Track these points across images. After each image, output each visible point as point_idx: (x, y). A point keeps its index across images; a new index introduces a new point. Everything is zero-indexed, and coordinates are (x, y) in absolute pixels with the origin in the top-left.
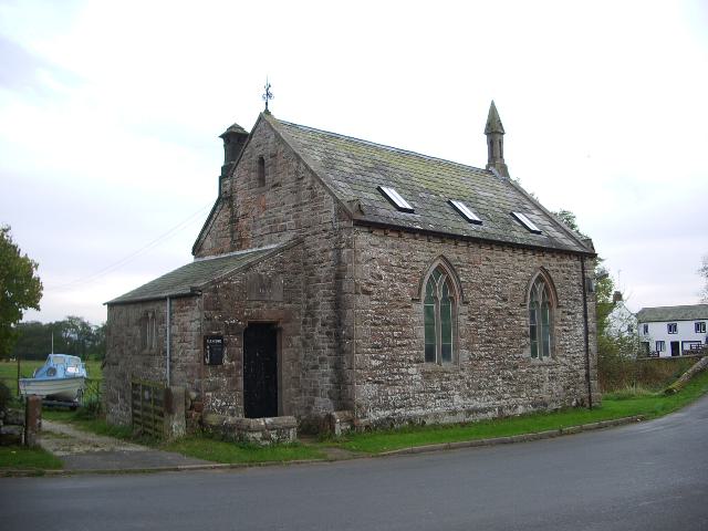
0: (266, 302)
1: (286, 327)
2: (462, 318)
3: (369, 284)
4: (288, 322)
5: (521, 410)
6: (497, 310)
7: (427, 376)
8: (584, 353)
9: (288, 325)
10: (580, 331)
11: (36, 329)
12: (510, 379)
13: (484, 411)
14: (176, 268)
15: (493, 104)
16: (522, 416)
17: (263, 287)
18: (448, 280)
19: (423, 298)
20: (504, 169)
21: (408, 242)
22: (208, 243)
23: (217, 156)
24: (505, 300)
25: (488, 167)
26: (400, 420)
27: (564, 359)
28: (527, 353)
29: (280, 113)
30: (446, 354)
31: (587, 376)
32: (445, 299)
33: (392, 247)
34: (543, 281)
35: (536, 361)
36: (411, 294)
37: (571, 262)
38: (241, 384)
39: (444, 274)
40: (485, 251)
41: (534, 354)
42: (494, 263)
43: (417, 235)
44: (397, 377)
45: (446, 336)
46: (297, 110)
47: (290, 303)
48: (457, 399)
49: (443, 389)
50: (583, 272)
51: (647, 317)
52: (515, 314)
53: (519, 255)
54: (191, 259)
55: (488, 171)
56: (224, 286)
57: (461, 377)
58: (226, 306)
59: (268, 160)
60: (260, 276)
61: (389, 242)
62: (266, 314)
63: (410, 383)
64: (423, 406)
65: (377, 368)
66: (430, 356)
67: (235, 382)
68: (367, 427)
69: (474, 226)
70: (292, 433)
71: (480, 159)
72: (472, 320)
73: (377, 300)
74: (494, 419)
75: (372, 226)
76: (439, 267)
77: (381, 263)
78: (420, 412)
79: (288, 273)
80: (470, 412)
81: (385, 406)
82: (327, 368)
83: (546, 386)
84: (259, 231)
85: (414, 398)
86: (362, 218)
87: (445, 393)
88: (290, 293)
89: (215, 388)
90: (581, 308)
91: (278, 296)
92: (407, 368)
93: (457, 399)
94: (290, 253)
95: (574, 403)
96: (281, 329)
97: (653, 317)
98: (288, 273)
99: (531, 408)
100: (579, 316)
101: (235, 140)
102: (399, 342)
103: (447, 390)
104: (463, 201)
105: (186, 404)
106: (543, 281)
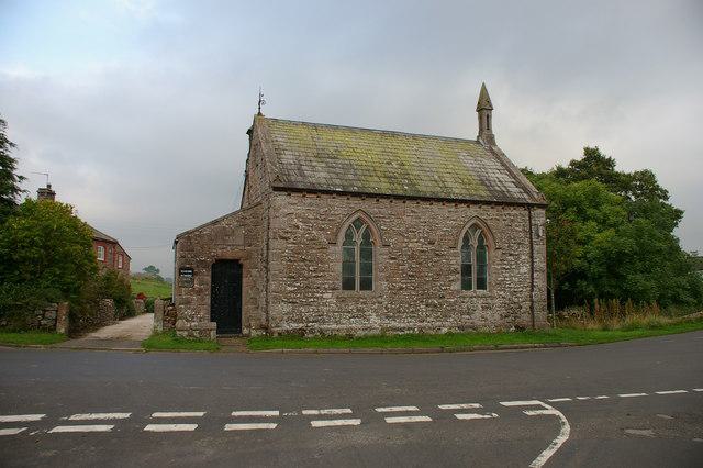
1: (246, 264)
5: (444, 330)
10: (525, 269)
12: (435, 306)
20: (491, 140)
24: (431, 243)
26: (311, 332)
28: (457, 286)
29: (267, 113)
30: (367, 285)
31: (532, 308)
35: (470, 293)
40: (411, 205)
41: (467, 286)
49: (358, 310)
53: (452, 207)
55: (478, 142)
63: (324, 305)
66: (348, 284)
68: (280, 334)
70: (213, 334)
71: (472, 132)
72: (392, 259)
75: (290, 190)
77: (298, 216)
78: (334, 326)
81: (300, 320)
83: (478, 314)
87: (361, 314)
88: (250, 239)
89: (188, 302)
90: (528, 250)
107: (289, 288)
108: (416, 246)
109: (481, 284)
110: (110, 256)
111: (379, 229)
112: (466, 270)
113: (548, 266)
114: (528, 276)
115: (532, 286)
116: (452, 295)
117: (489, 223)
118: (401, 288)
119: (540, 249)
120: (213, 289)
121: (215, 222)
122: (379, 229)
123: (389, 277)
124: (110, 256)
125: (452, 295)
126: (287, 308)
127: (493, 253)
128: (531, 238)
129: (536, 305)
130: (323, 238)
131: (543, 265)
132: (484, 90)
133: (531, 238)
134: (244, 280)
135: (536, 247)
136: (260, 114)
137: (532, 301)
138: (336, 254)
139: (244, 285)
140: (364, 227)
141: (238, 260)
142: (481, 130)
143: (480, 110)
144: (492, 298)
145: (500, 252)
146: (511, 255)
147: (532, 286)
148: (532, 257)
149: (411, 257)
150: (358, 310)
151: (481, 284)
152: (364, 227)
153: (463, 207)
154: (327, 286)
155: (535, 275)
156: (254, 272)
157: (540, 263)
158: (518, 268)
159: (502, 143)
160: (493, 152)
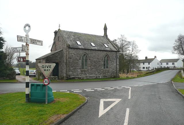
2: (89, 62)
5: (101, 77)
7: (82, 71)
10: (115, 64)
11: (101, 117)
13: (93, 77)
14: (46, 54)
15: (105, 25)
16: (101, 78)
18: (86, 56)
19: (81, 59)
20: (107, 36)
22: (53, 50)
23: (53, 35)
24: (98, 59)
28: (103, 68)
29: (62, 29)
31: (116, 72)
32: (107, 60)
34: (107, 56)
37: (113, 53)
41: (104, 68)
45: (107, 65)
46: (65, 28)
48: (88, 75)
49: (85, 73)
51: (162, 61)
54: (50, 52)
55: (104, 36)
59: (59, 37)
61: (75, 50)
64: (81, 76)
65: (72, 69)
71: (102, 34)
74: (95, 78)
76: (85, 54)
78: (80, 76)
80: (90, 77)
82: (65, 70)
84: (58, 48)
90: (116, 61)
91: (59, 58)
93: (88, 75)
95: (113, 76)
96: (59, 64)
97: (163, 61)
99: (103, 77)
101: (56, 33)
104: (93, 42)
106: (107, 56)
109: (107, 68)
112: (104, 65)
116: (102, 70)
119: (118, 60)
126: (72, 73)
127: (109, 61)
131: (119, 64)
135: (117, 60)
136: (59, 29)
138: (81, 61)
140: (85, 56)
148: (116, 62)
152: (85, 56)
156: (61, 65)
157: (118, 63)
159: (109, 37)
160: (107, 39)
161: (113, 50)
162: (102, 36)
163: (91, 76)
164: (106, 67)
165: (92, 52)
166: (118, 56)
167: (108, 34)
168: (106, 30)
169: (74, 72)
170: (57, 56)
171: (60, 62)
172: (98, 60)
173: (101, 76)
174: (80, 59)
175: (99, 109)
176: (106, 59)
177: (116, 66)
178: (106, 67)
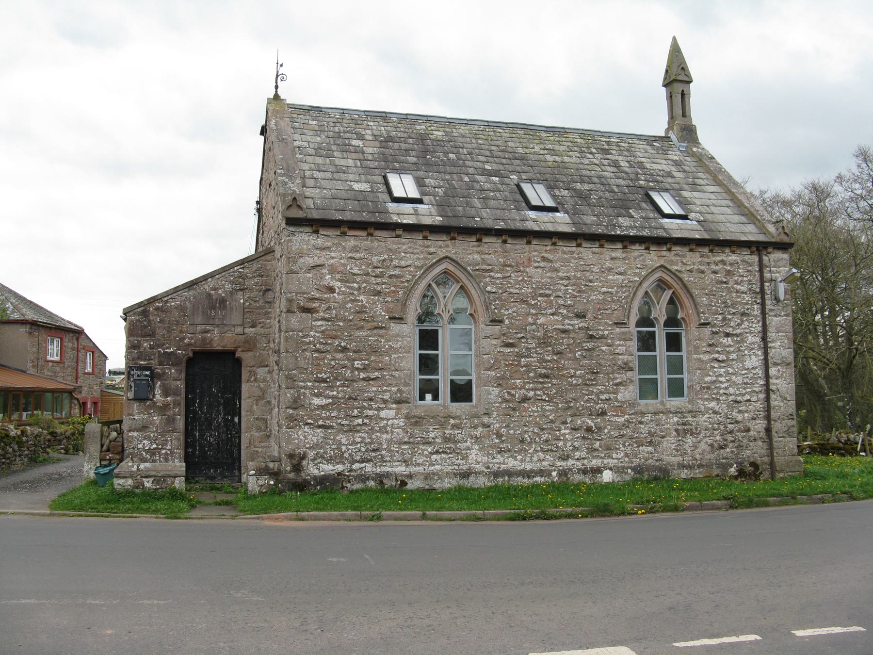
0: (218, 326)
1: (247, 358)
3: (313, 299)
4: (249, 350)
6: (564, 331)
7: (415, 421)
8: (762, 396)
9: (250, 354)
10: (754, 361)
12: (589, 430)
17: (213, 308)
20: (689, 133)
21: (384, 242)
24: (581, 316)
25: (667, 131)
27: (712, 404)
29: (292, 95)
31: (768, 430)
33: (355, 249)
35: (649, 404)
36: (388, 311)
37: (733, 257)
38: (180, 423)
39: (670, 288)
41: (648, 389)
42: (557, 265)
43: (770, 250)
44: (360, 421)
47: (253, 327)
50: (761, 271)
52: (602, 337)
56: (157, 309)
57: (485, 426)
58: (160, 332)
60: (209, 295)
61: (351, 242)
62: (219, 340)
63: (383, 430)
65: (322, 407)
67: (171, 420)
69: (408, 207)
73: (324, 319)
75: (317, 225)
76: (446, 272)
77: (333, 271)
78: (401, 469)
79: (251, 290)
81: (339, 458)
83: (670, 443)
85: (388, 450)
86: (300, 214)
90: (758, 327)
91: (236, 318)
92: (379, 409)
94: (255, 266)
95: (733, 471)
98: (251, 290)
100: (753, 339)
102: (362, 375)
103: (456, 442)
105: (102, 446)
107: (316, 401)
108: (552, 322)
109: (676, 389)
110: (70, 354)
111: (483, 291)
113: (798, 349)
114: (760, 372)
115: (768, 390)
116: (620, 409)
117: (685, 277)
118: (525, 399)
120: (189, 403)
121: (191, 285)
122: (483, 291)
123: (503, 378)
124: (70, 354)
125: (620, 409)
127: (694, 332)
128: (763, 304)
129: (776, 426)
130: (380, 311)
131: (788, 353)
132: (675, 52)
133: (763, 304)
134: (245, 387)
135: (773, 321)
136: (277, 97)
137: (768, 418)
139: (244, 395)
141: (233, 353)
142: (672, 117)
143: (668, 84)
144: (694, 413)
145: (707, 330)
146: (727, 335)
147: (768, 390)
148: (764, 339)
149: (544, 342)
150: (447, 440)
151: (676, 389)
152: (667, 295)
153: (637, 250)
154: (387, 396)
155: (773, 371)
156: (261, 372)
158: (741, 359)
161: (728, 237)
162: (650, 140)
163: (511, 463)
164: (663, 387)
165: (518, 250)
166: (775, 290)
167: (697, 115)
168: (678, 87)
169: (341, 429)
170: (223, 301)
171: (250, 344)
172: (578, 323)
173: (612, 462)
174: (400, 319)
175: (836, 633)
176: (660, 313)
177: (767, 377)
178: (663, 387)
